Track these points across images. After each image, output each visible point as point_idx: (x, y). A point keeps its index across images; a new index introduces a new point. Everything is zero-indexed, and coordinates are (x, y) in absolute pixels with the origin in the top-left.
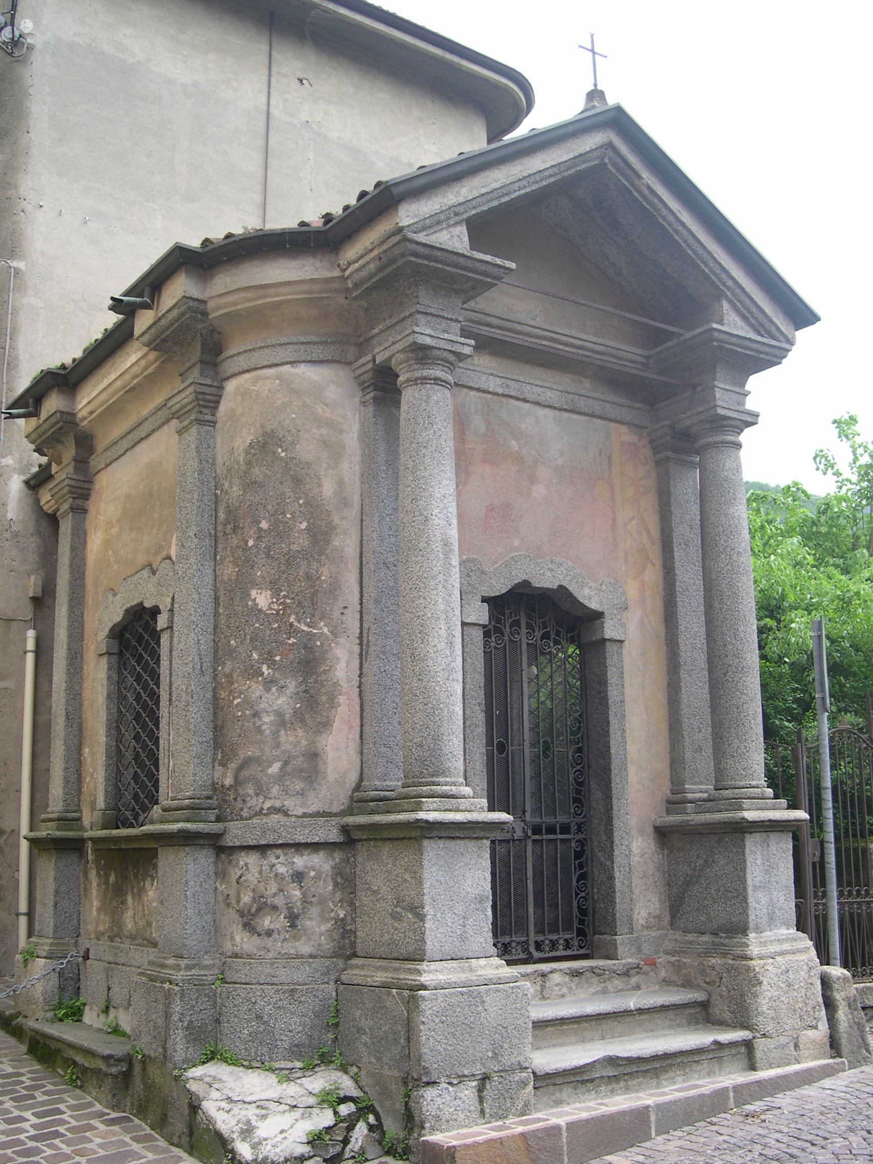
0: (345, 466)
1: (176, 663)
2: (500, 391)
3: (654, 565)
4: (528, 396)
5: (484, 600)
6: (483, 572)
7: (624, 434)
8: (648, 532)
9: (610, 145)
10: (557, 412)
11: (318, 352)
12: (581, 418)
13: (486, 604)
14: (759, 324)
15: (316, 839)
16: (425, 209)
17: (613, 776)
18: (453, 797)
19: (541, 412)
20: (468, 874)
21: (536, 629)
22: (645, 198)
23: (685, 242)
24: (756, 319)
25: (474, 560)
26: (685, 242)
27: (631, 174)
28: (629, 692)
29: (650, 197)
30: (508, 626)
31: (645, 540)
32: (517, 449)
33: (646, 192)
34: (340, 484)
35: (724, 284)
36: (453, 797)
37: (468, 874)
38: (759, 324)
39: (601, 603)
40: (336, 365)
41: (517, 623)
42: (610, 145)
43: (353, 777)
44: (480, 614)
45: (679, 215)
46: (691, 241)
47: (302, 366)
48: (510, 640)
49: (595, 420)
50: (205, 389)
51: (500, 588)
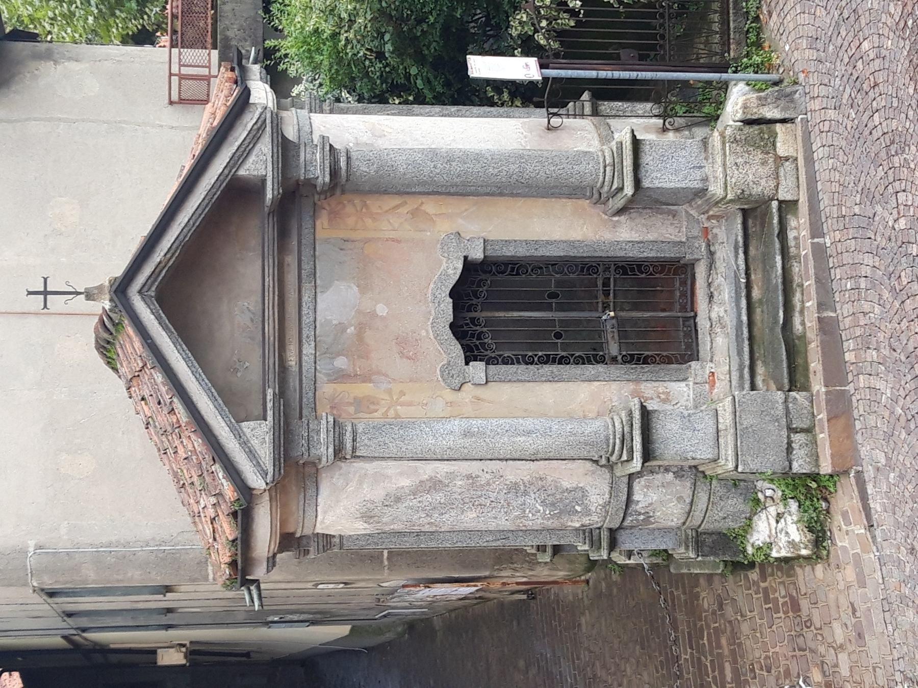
0: (389, 472)
1: (258, 286)
2: (313, 344)
3: (422, 203)
4: (312, 319)
5: (467, 363)
6: (449, 364)
7: (322, 222)
8: (397, 207)
9: (140, 292)
10: (318, 290)
11: (311, 492)
12: (317, 266)
13: (471, 363)
14: (255, 137)
15: (626, 489)
16: (248, 467)
17: (579, 255)
18: (623, 435)
19: (320, 307)
20: (668, 427)
21: (471, 302)
22: (173, 254)
23: (200, 215)
24: (250, 143)
25: (442, 372)
26: (200, 215)
27: (157, 270)
28: (518, 234)
29: (172, 251)
30: (475, 328)
31: (404, 210)
32: (353, 328)
33: (168, 256)
34: (401, 474)
35: (227, 176)
36: (623, 435)
37: (668, 427)
38: (255, 137)
39: (459, 259)
40: (319, 479)
41: (473, 320)
42: (140, 292)
43: (588, 464)
44: (477, 369)
45: (183, 225)
46: (199, 211)
47: (319, 500)
48: (484, 326)
49: (317, 253)
50: (321, 547)
51: (457, 350)
